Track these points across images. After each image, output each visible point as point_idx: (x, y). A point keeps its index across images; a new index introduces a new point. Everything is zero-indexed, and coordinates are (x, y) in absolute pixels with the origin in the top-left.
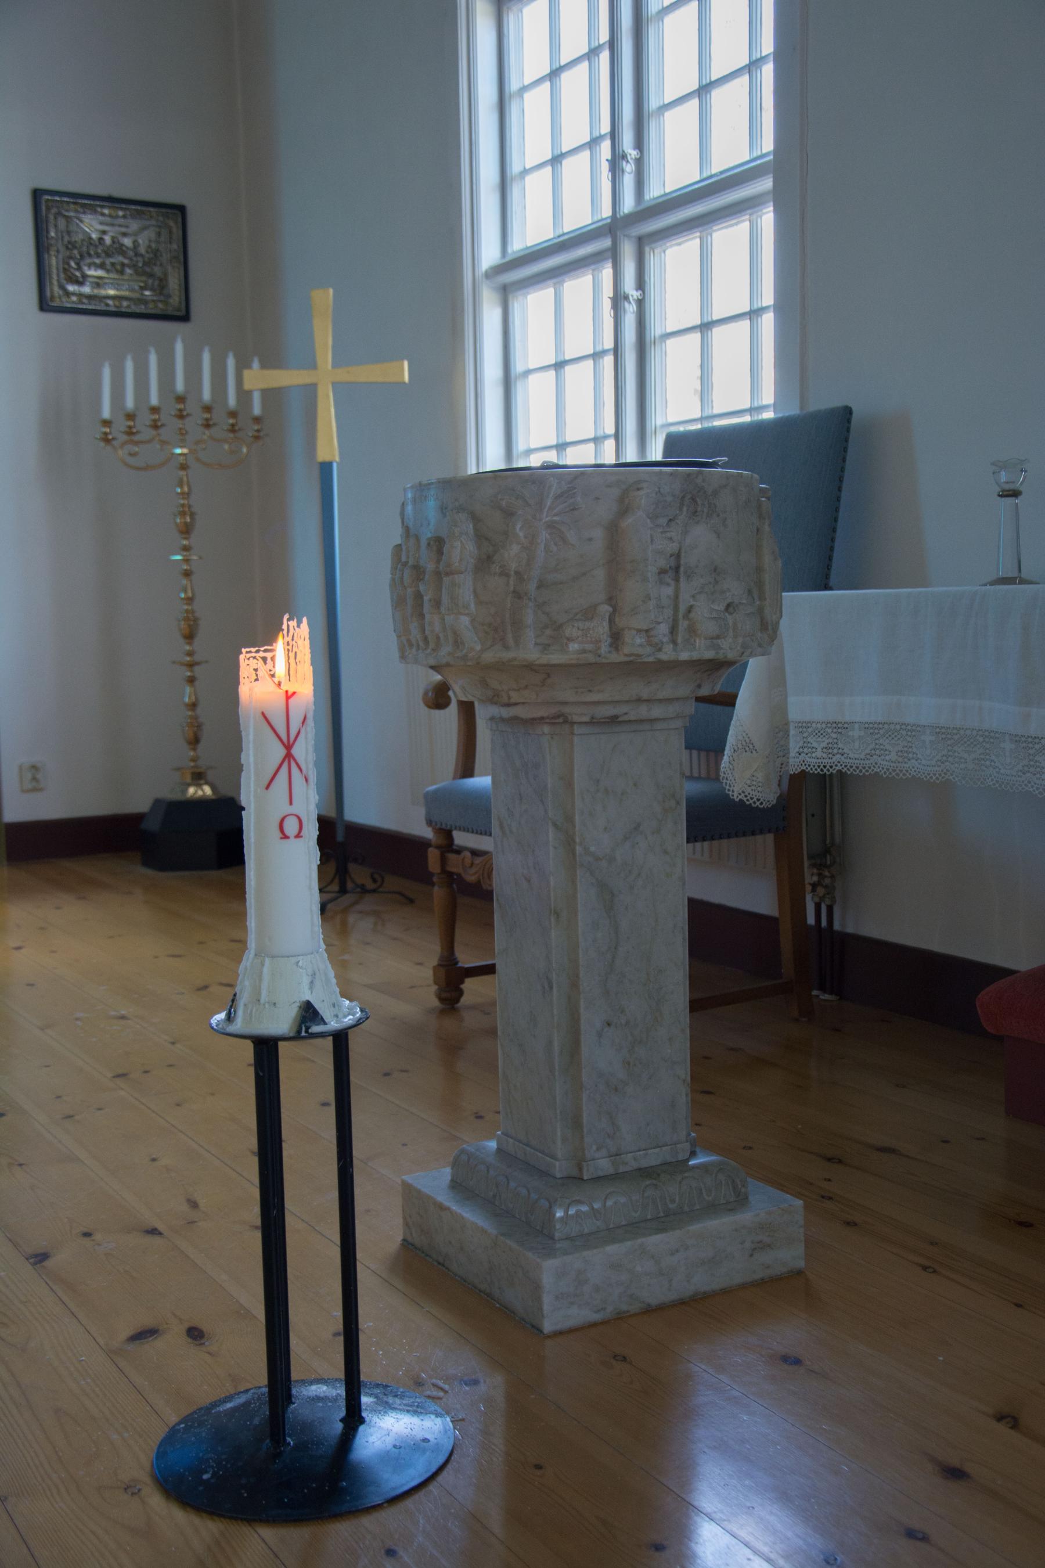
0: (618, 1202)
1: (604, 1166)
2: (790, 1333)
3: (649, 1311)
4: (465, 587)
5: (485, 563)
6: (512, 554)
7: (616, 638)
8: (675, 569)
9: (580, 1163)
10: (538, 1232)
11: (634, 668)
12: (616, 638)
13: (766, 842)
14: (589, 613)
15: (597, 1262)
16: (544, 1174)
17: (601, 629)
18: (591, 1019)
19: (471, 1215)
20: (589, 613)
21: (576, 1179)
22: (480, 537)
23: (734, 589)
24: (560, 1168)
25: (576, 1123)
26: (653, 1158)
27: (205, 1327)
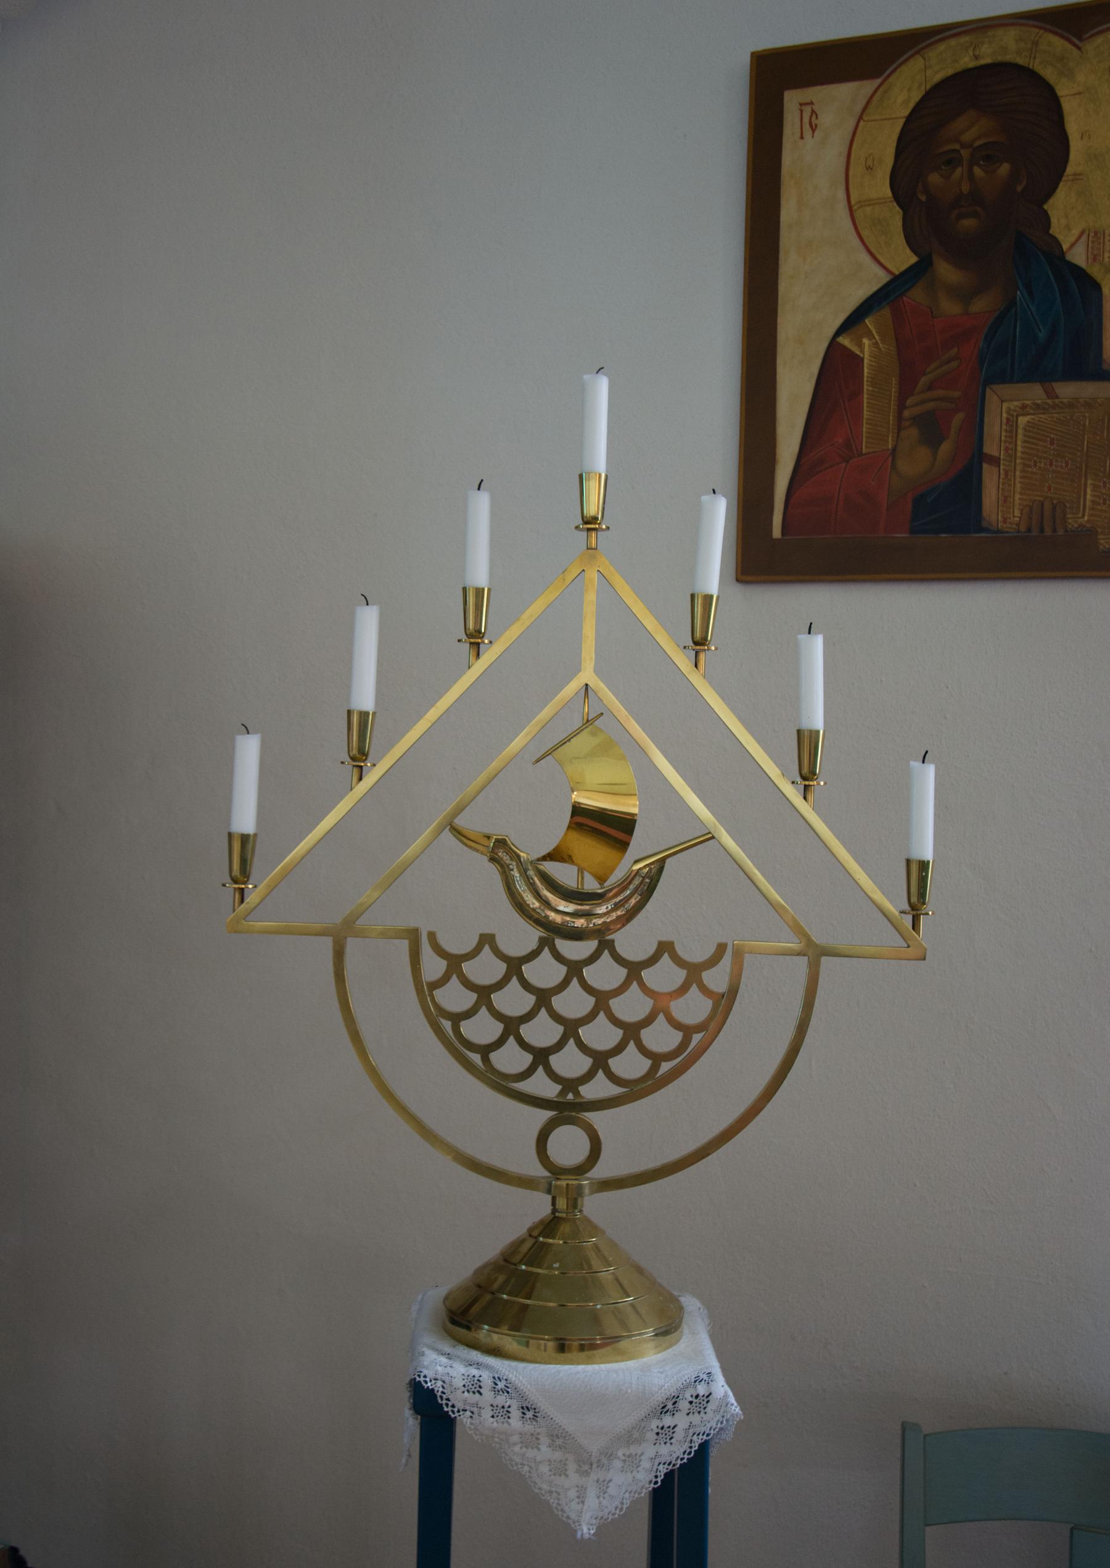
13: (792, 99)
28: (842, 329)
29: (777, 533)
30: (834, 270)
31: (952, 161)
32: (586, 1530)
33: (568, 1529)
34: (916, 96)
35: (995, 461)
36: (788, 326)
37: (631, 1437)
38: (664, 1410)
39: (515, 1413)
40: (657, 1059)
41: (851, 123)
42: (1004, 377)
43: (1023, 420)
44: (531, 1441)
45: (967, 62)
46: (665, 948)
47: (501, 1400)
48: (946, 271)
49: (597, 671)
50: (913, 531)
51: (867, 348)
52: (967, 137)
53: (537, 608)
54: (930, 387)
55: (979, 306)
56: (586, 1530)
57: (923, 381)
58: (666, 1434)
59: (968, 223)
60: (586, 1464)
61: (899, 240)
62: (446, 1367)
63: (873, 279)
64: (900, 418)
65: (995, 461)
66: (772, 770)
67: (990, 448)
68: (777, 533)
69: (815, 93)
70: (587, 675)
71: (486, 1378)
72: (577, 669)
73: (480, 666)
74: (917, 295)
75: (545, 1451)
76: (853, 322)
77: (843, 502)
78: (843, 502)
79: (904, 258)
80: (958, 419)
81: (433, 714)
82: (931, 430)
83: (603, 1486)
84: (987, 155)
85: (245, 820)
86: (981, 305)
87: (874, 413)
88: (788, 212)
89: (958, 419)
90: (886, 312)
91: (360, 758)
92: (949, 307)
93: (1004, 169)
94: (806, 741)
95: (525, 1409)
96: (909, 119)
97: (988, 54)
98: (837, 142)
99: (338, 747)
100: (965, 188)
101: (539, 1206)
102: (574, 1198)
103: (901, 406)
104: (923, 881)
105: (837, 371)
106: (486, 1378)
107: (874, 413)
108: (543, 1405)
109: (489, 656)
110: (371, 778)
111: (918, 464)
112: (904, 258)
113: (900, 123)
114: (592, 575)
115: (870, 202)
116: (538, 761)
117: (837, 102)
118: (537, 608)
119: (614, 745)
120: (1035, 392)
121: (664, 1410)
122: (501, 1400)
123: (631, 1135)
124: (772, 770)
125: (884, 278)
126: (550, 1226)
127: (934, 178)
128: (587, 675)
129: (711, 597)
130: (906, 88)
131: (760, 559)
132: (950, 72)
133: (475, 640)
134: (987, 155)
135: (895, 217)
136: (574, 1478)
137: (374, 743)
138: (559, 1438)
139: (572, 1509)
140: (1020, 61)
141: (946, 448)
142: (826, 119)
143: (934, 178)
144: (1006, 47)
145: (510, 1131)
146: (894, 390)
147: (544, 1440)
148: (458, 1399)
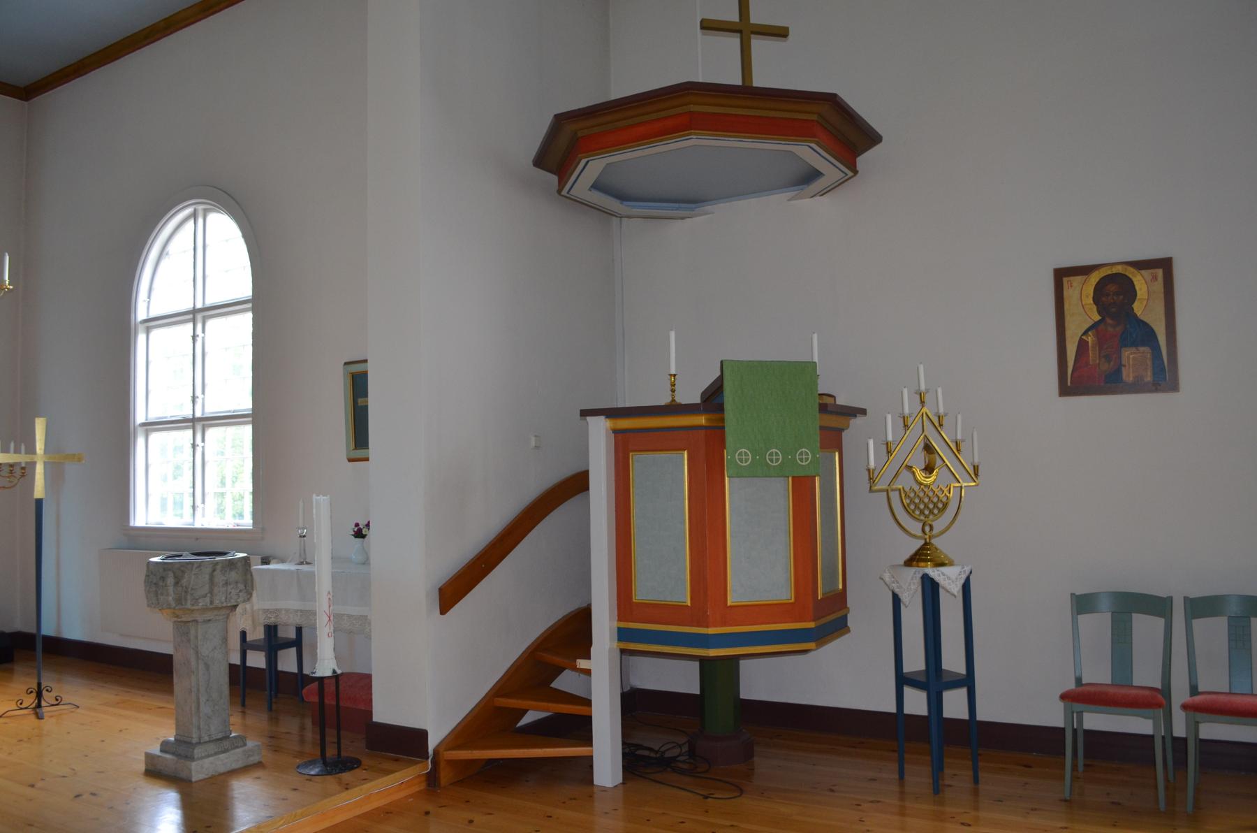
0: (212, 748)
1: (207, 739)
2: (259, 773)
3: (221, 774)
4: (171, 589)
5: (176, 584)
6: (184, 582)
7: (212, 603)
8: (226, 584)
9: (200, 738)
10: (190, 758)
11: (217, 608)
12: (212, 603)
13: (1065, 280)
14: (205, 596)
15: (207, 762)
16: (190, 743)
17: (208, 600)
18: (203, 699)
19: (168, 756)
20: (205, 596)
21: (199, 743)
22: (175, 577)
23: (241, 586)
24: (195, 740)
25: (199, 728)
26: (220, 736)
27: (351, 529)
36: (1068, 333)
48: (1109, 321)
51: (1090, 339)
63: (1090, 323)
69: (1072, 278)
76: (1085, 333)
79: (1097, 318)
87: (1093, 356)
88: (1066, 306)
92: (1110, 329)
98: (1081, 294)
101: (919, 544)
105: (1082, 345)
116: (360, 436)
117: (1077, 280)
120: (1134, 350)
123: (939, 524)
130: (1094, 278)
138: (949, 578)
142: (1075, 284)
145: (915, 527)
148: (937, 579)
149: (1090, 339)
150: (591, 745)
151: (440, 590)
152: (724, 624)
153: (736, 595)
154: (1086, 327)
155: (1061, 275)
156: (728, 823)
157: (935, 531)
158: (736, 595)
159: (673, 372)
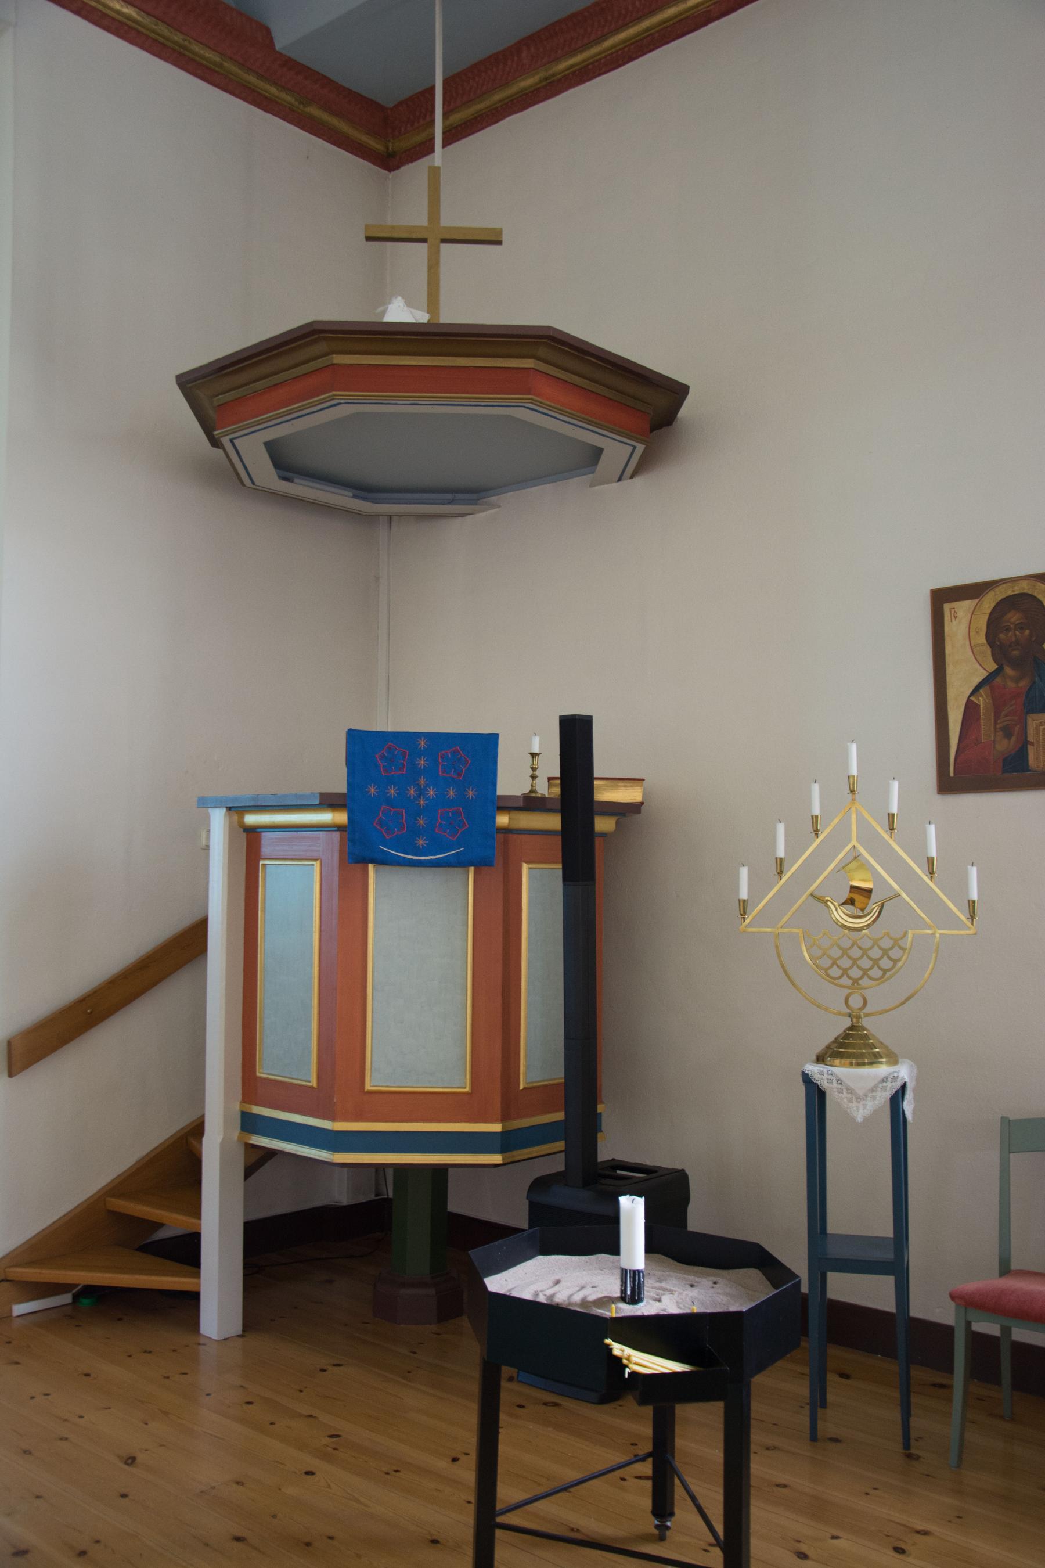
13: (947, 607)
28: (972, 694)
29: (952, 774)
30: (967, 672)
31: (1008, 629)
32: (859, 1119)
33: (853, 1119)
34: (993, 605)
35: (1032, 744)
36: (951, 693)
37: (873, 1090)
38: (883, 1081)
39: (835, 1081)
40: (885, 971)
41: (969, 616)
42: (1032, 711)
43: (1042, 727)
44: (840, 1091)
45: (1010, 593)
46: (887, 934)
47: (830, 1077)
48: (1008, 671)
49: (858, 840)
50: (1003, 772)
51: (981, 701)
52: (1013, 620)
53: (836, 821)
54: (1006, 716)
55: (1022, 684)
56: (859, 1119)
57: (1003, 713)
58: (884, 1089)
59: (1016, 653)
60: (858, 1099)
61: (991, 659)
62: (814, 1070)
63: (982, 674)
64: (995, 728)
65: (1032, 744)
66: (919, 871)
67: (1030, 739)
68: (952, 774)
69: (956, 605)
70: (854, 842)
71: (825, 1071)
72: (850, 841)
73: (818, 841)
74: (998, 680)
75: (845, 1094)
77: (977, 761)
78: (977, 761)
79: (993, 666)
80: (1017, 728)
81: (804, 857)
82: (1007, 732)
83: (865, 1106)
84: (1021, 627)
85: (744, 894)
86: (1024, 684)
87: (986, 727)
89: (1017, 728)
90: (987, 687)
91: (780, 873)
92: (1011, 684)
93: (1027, 632)
94: (930, 861)
95: (838, 1080)
96: (991, 614)
97: (1017, 590)
98: (964, 623)
99: (773, 869)
100: (1014, 639)
101: (847, 1023)
102: (858, 1017)
103: (996, 723)
104: (974, 907)
105: (971, 711)
106: (825, 1071)
107: (986, 727)
108: (844, 1079)
109: (821, 837)
110: (784, 879)
111: (1004, 746)
112: (993, 666)
113: (987, 616)
114: (853, 809)
115: (977, 645)
117: (963, 608)
118: (836, 821)
119: (865, 866)
121: (883, 1081)
122: (830, 1077)
124: (919, 871)
125: (985, 674)
126: (852, 1028)
127: (1002, 636)
128: (854, 842)
129: (893, 815)
130: (989, 602)
131: (947, 785)
132: (1004, 596)
133: (816, 832)
134: (1021, 627)
135: (988, 651)
136: (855, 1104)
137: (785, 868)
138: (850, 1090)
139: (855, 1114)
140: (1030, 592)
141: (1013, 739)
142: (960, 614)
143: (1002, 636)
144: (1024, 587)
146: (992, 717)
147: (845, 1091)
148: (825, 1085)
149: (981, 701)
150: (198, 1275)
151: (9, 1043)
152: (359, 1117)
153: (377, 1078)
154: (976, 680)
155: (941, 598)
156: (305, 1410)
157: (867, 1010)
158: (377, 1078)
159: (536, 750)
